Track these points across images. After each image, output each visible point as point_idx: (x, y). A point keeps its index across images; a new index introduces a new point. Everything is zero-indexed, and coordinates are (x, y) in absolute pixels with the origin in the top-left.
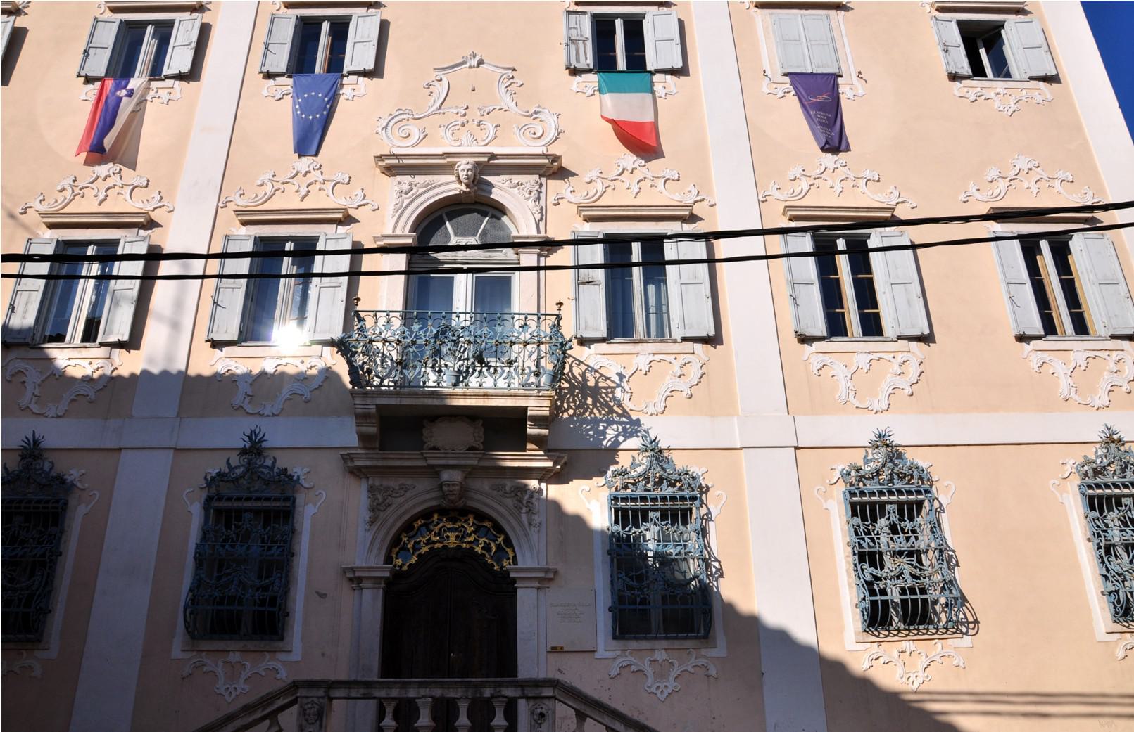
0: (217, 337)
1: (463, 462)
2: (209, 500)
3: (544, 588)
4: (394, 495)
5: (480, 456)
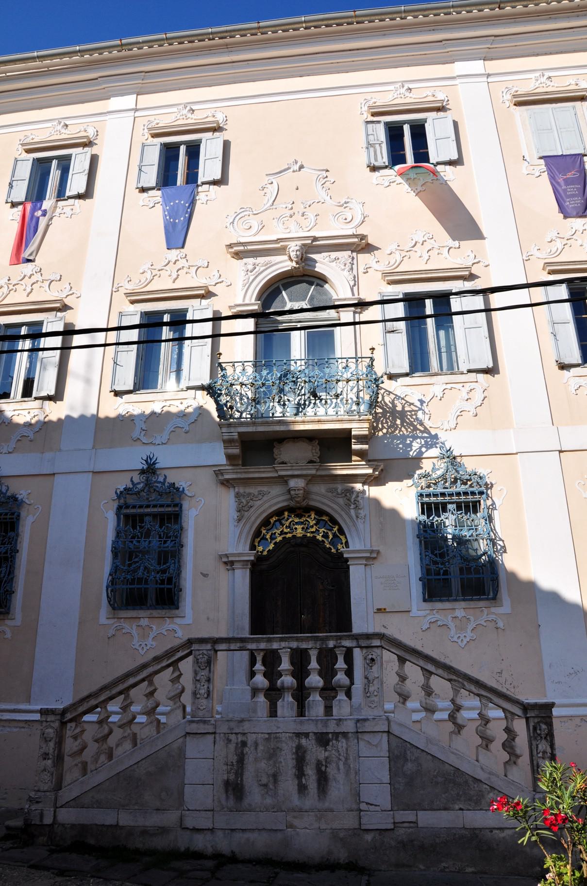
0: (118, 388)
1: (305, 472)
2: (120, 508)
3: (370, 565)
4: (254, 499)
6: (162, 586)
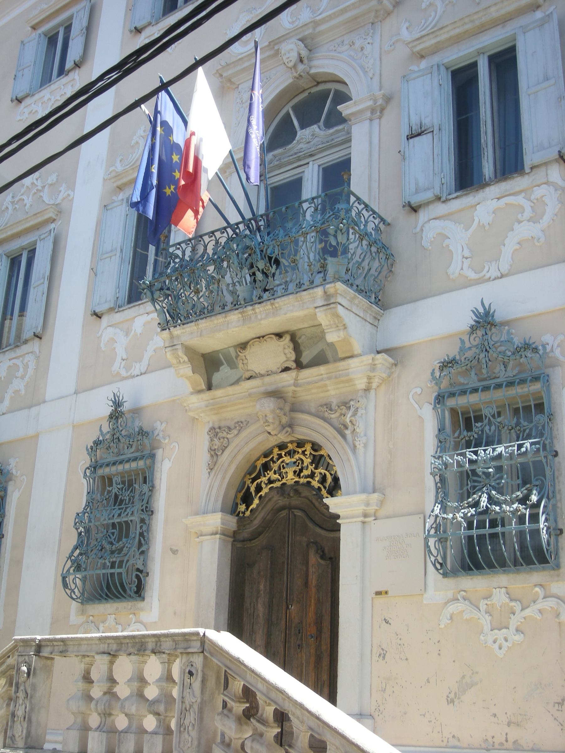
2: (440, 399)
6: (112, 571)
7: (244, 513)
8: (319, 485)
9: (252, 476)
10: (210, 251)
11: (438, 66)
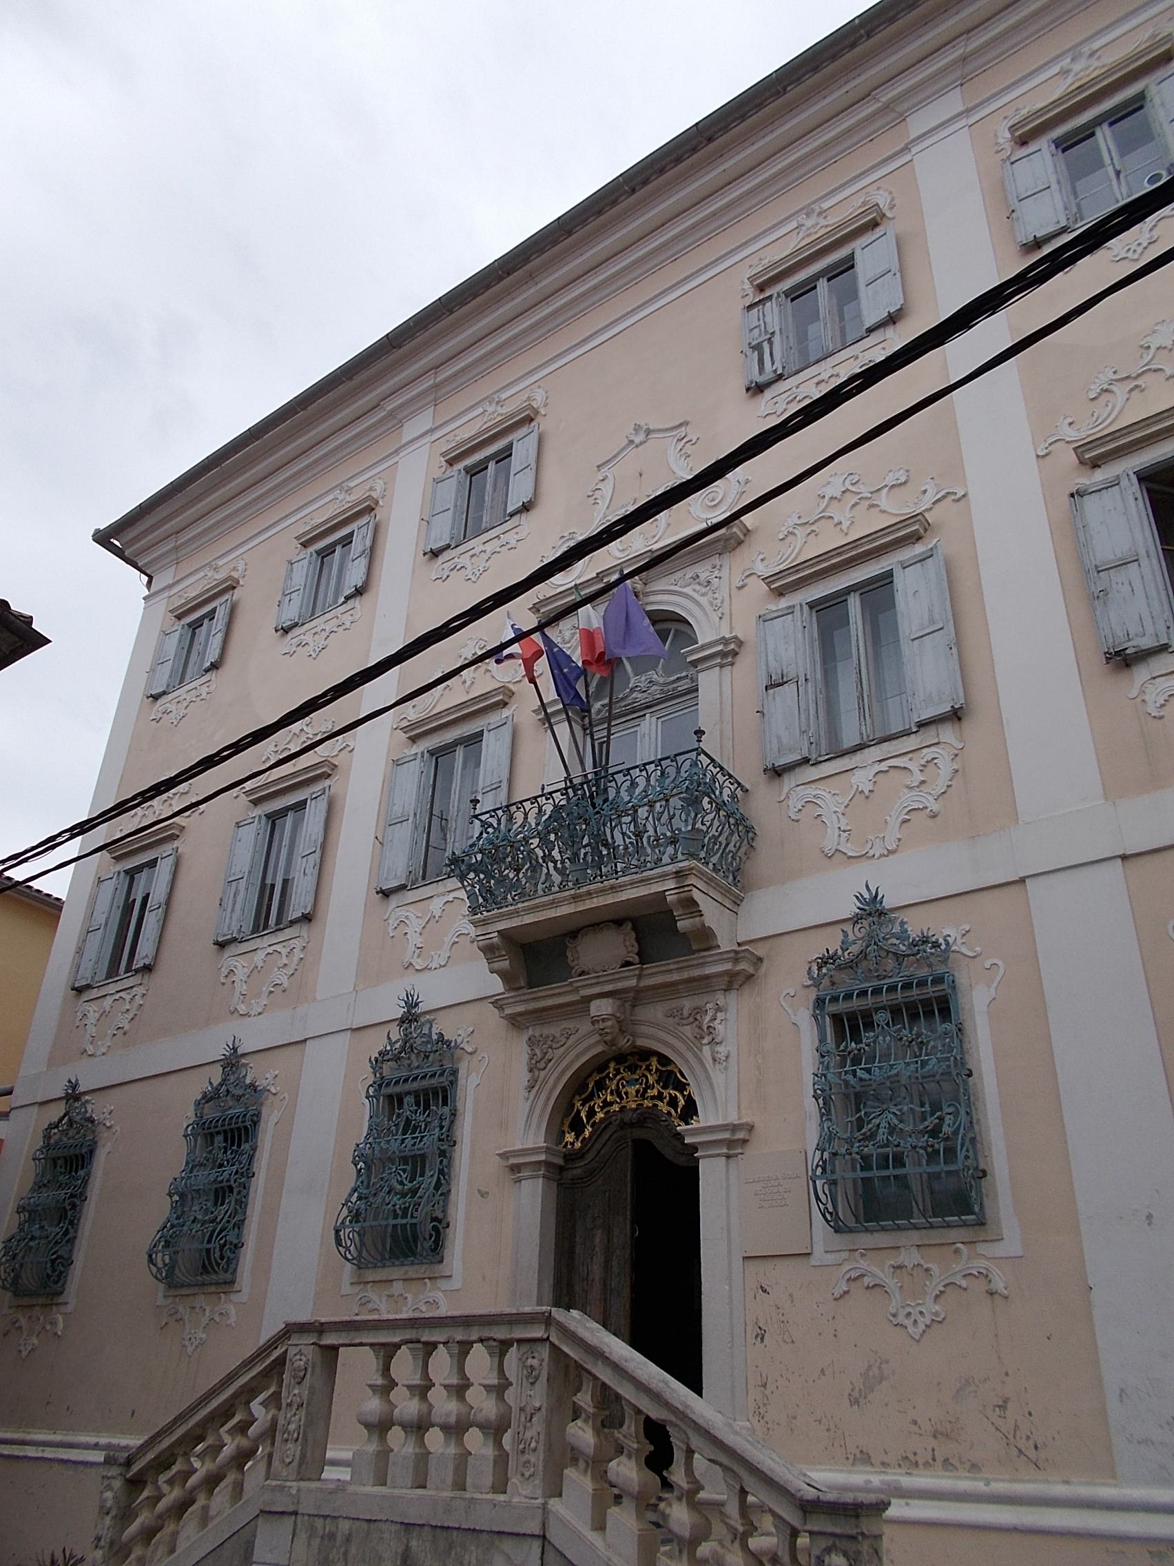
1: (620, 985)
2: (819, 1003)
3: (736, 1155)
4: (554, 1046)
5: (637, 972)
7: (572, 1144)
8: (669, 1108)
9: (583, 1096)
10: (532, 820)
11: (801, 605)
